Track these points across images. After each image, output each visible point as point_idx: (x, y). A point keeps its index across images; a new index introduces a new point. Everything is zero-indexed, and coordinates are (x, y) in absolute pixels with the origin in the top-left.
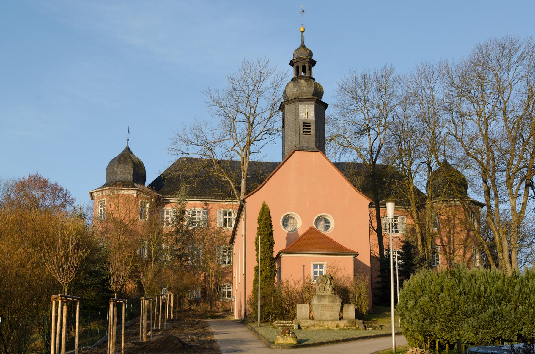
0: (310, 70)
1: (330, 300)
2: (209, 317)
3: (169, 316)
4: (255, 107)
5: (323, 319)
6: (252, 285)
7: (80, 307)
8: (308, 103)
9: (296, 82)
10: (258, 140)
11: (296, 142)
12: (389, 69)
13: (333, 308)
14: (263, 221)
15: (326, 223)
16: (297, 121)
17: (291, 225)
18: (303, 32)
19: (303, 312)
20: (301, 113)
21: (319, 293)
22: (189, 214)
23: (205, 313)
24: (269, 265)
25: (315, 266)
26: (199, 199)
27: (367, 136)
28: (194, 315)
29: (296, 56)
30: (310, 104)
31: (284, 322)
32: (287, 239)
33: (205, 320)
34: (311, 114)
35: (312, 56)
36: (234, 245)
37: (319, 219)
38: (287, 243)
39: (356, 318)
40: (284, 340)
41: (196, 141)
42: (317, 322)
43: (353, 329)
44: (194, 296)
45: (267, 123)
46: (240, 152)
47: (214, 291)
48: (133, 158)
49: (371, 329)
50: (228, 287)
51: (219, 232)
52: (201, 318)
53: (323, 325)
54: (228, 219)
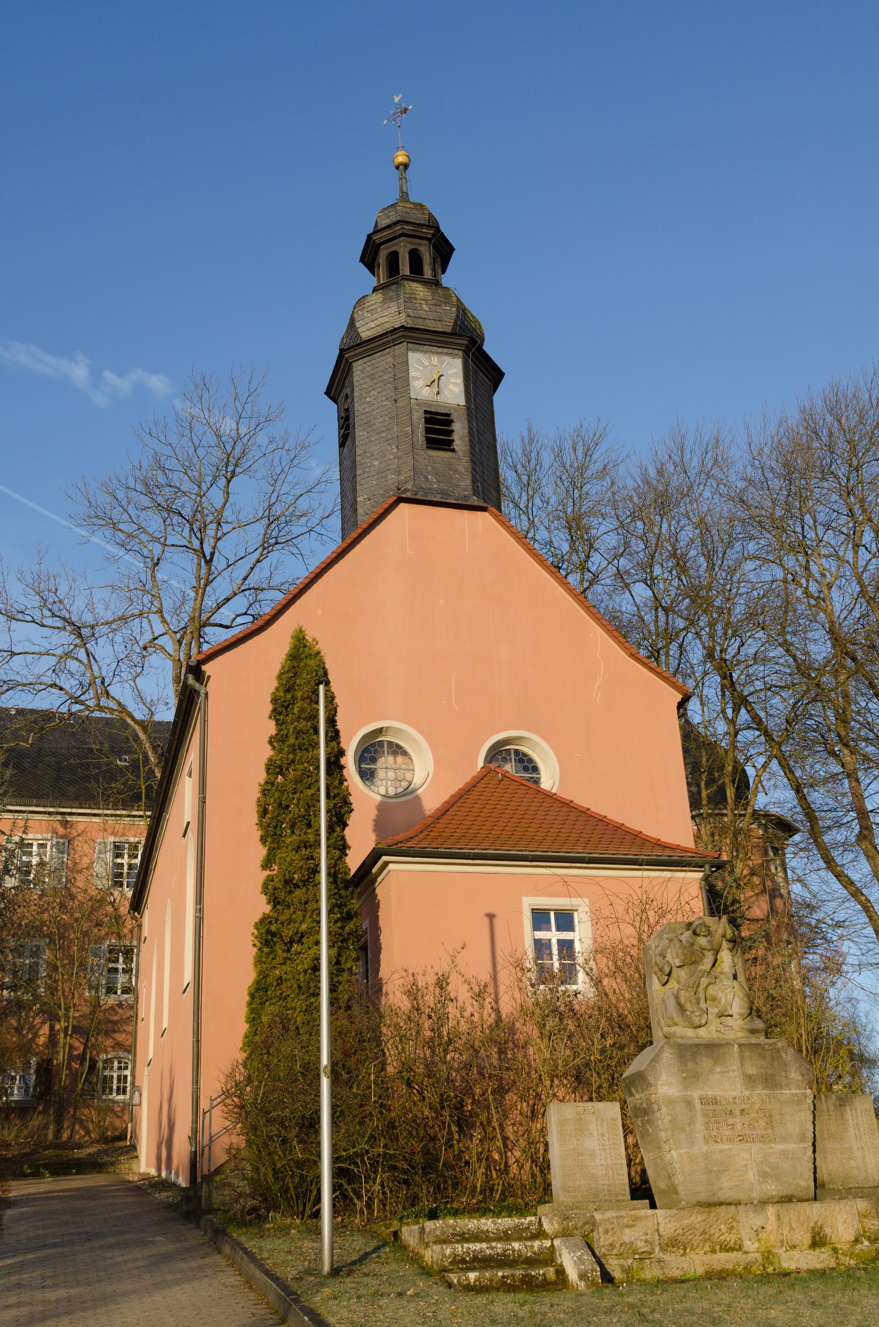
1: (751, 1070)
2: (46, 1166)
5: (722, 1196)
6: (242, 1010)
8: (440, 350)
11: (399, 473)
15: (526, 769)
16: (400, 404)
18: (406, 166)
19: (593, 1155)
20: (417, 378)
25: (540, 918)
26: (44, 806)
30: (447, 354)
31: (487, 1224)
34: (451, 387)
36: (147, 913)
37: (497, 752)
42: (696, 1218)
50: (120, 1062)
51: (99, 902)
53: (731, 1238)
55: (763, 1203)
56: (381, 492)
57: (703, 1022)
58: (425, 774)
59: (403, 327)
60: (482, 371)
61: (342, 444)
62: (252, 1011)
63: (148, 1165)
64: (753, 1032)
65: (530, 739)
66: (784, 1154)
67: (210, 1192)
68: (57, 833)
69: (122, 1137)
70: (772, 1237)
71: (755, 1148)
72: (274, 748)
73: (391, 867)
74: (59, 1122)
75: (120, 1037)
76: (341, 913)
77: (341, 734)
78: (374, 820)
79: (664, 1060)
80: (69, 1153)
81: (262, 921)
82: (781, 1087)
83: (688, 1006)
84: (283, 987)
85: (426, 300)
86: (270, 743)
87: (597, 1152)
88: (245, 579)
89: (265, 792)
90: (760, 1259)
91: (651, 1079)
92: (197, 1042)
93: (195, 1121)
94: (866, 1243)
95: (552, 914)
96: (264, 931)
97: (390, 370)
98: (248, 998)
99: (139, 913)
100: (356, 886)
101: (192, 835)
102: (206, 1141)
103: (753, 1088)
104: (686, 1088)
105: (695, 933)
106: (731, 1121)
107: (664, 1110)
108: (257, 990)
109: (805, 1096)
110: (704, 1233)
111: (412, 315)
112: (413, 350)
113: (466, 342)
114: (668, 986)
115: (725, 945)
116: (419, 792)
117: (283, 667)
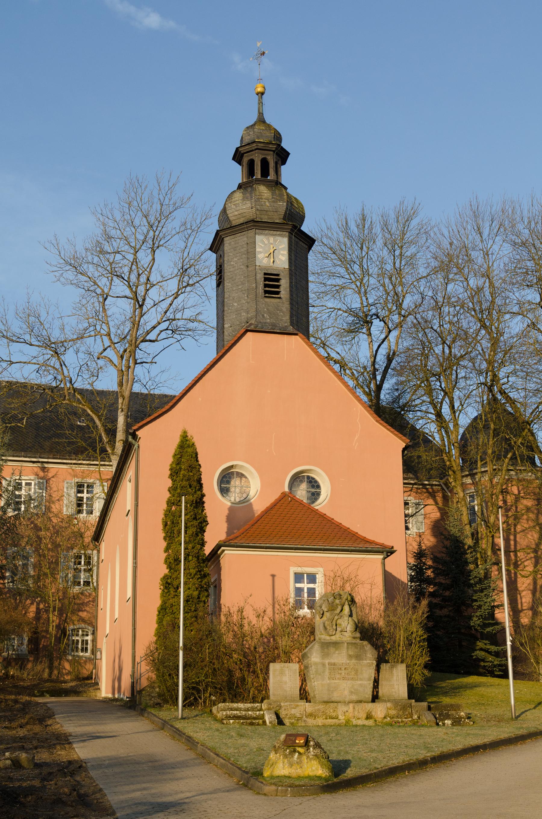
0: (277, 172)
1: (351, 653)
2: (47, 692)
4: (148, 270)
5: (333, 699)
8: (275, 233)
9: (249, 189)
10: (151, 341)
11: (248, 313)
12: (409, 208)
13: (357, 671)
14: (182, 472)
15: (313, 487)
16: (250, 269)
17: (238, 490)
18: (262, 94)
19: (286, 683)
20: (260, 252)
21: (323, 637)
22: (9, 485)
23: (39, 684)
24: (196, 574)
25: (299, 577)
26: (29, 457)
27: (365, 336)
29: (247, 140)
32: (229, 519)
33: (40, 700)
34: (280, 257)
35: (281, 142)
37: (297, 478)
38: (228, 529)
39: (410, 697)
40: (291, 765)
41: (27, 337)
42: (321, 707)
43: (405, 725)
44: (14, 650)
45: (171, 305)
46: (116, 360)
47: (58, 640)
49: (448, 722)
50: (83, 631)
52: (29, 695)
53: (334, 714)
55: (349, 702)
56: (238, 323)
57: (334, 634)
58: (256, 490)
59: (253, 221)
60: (301, 241)
61: (218, 285)
62: (159, 619)
63: (106, 693)
64: (354, 638)
65: (315, 471)
66: (361, 685)
67: (140, 698)
68: (38, 475)
69: (90, 677)
70: (350, 714)
71: (349, 682)
72: (171, 493)
73: (226, 552)
74: (51, 668)
75: (83, 614)
76: (200, 575)
77: (204, 486)
78: (227, 516)
79: (315, 648)
80: (58, 685)
81: (164, 577)
82: (363, 660)
83: (328, 627)
84: (174, 608)
85: (268, 199)
86: (169, 490)
87: (288, 682)
88: (166, 312)
89: (166, 515)
90: (344, 723)
91: (309, 655)
92: (134, 629)
93: (133, 667)
94: (389, 719)
95: (305, 575)
96: (165, 582)
97: (245, 246)
98: (157, 613)
99: (98, 542)
100: (209, 561)
101: (131, 517)
102: (139, 677)
103: (351, 660)
104: (323, 659)
105: (334, 598)
106: (340, 672)
107: (313, 667)
108: (162, 609)
109: (373, 663)
110: (323, 712)
111: (259, 209)
112: (260, 234)
113: (291, 227)
114: (322, 619)
115: (347, 603)
116: (252, 501)
117: (176, 452)
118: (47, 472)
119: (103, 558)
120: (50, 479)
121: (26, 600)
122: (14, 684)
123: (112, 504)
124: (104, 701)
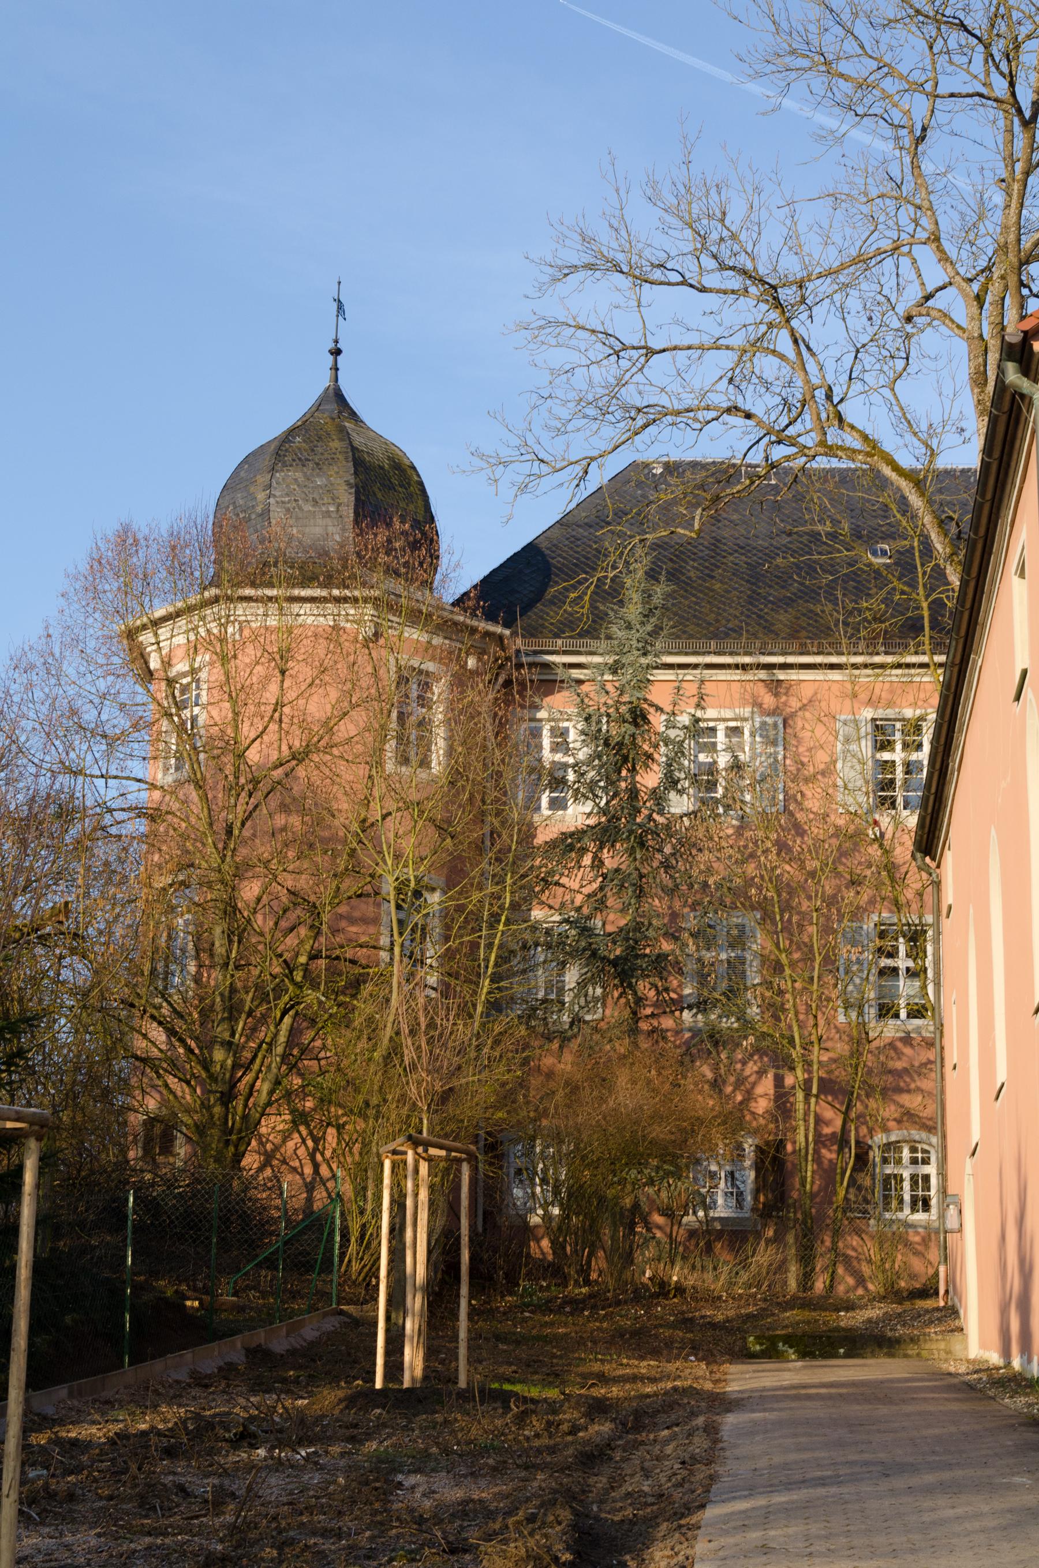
2: (788, 1340)
3: (394, 1367)
7: (404, 1262)
23: (762, 1314)
28: (686, 1322)
36: (949, 859)
48: (358, 440)
50: (914, 1150)
54: (899, 770)
63: (983, 1345)
74: (806, 1258)
75: (911, 1101)
80: (830, 1317)
99: (933, 859)
118: (786, 694)
119: (950, 901)
120: (793, 715)
121: (744, 1063)
122: (683, 1313)
123: (967, 698)
124: (970, 1387)
